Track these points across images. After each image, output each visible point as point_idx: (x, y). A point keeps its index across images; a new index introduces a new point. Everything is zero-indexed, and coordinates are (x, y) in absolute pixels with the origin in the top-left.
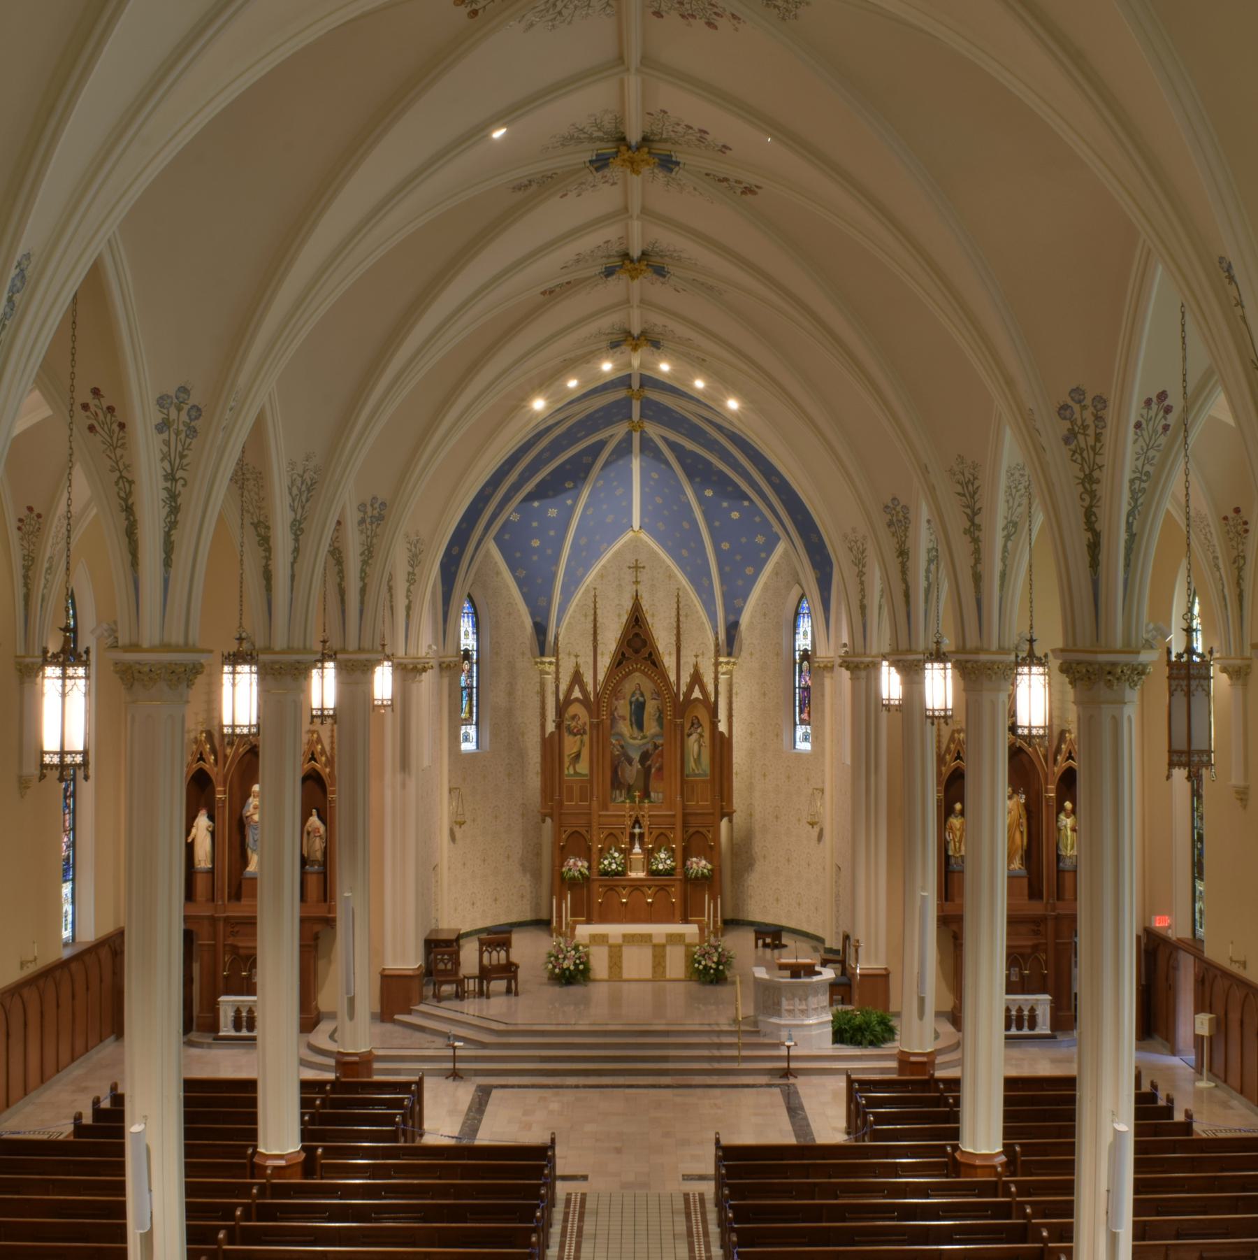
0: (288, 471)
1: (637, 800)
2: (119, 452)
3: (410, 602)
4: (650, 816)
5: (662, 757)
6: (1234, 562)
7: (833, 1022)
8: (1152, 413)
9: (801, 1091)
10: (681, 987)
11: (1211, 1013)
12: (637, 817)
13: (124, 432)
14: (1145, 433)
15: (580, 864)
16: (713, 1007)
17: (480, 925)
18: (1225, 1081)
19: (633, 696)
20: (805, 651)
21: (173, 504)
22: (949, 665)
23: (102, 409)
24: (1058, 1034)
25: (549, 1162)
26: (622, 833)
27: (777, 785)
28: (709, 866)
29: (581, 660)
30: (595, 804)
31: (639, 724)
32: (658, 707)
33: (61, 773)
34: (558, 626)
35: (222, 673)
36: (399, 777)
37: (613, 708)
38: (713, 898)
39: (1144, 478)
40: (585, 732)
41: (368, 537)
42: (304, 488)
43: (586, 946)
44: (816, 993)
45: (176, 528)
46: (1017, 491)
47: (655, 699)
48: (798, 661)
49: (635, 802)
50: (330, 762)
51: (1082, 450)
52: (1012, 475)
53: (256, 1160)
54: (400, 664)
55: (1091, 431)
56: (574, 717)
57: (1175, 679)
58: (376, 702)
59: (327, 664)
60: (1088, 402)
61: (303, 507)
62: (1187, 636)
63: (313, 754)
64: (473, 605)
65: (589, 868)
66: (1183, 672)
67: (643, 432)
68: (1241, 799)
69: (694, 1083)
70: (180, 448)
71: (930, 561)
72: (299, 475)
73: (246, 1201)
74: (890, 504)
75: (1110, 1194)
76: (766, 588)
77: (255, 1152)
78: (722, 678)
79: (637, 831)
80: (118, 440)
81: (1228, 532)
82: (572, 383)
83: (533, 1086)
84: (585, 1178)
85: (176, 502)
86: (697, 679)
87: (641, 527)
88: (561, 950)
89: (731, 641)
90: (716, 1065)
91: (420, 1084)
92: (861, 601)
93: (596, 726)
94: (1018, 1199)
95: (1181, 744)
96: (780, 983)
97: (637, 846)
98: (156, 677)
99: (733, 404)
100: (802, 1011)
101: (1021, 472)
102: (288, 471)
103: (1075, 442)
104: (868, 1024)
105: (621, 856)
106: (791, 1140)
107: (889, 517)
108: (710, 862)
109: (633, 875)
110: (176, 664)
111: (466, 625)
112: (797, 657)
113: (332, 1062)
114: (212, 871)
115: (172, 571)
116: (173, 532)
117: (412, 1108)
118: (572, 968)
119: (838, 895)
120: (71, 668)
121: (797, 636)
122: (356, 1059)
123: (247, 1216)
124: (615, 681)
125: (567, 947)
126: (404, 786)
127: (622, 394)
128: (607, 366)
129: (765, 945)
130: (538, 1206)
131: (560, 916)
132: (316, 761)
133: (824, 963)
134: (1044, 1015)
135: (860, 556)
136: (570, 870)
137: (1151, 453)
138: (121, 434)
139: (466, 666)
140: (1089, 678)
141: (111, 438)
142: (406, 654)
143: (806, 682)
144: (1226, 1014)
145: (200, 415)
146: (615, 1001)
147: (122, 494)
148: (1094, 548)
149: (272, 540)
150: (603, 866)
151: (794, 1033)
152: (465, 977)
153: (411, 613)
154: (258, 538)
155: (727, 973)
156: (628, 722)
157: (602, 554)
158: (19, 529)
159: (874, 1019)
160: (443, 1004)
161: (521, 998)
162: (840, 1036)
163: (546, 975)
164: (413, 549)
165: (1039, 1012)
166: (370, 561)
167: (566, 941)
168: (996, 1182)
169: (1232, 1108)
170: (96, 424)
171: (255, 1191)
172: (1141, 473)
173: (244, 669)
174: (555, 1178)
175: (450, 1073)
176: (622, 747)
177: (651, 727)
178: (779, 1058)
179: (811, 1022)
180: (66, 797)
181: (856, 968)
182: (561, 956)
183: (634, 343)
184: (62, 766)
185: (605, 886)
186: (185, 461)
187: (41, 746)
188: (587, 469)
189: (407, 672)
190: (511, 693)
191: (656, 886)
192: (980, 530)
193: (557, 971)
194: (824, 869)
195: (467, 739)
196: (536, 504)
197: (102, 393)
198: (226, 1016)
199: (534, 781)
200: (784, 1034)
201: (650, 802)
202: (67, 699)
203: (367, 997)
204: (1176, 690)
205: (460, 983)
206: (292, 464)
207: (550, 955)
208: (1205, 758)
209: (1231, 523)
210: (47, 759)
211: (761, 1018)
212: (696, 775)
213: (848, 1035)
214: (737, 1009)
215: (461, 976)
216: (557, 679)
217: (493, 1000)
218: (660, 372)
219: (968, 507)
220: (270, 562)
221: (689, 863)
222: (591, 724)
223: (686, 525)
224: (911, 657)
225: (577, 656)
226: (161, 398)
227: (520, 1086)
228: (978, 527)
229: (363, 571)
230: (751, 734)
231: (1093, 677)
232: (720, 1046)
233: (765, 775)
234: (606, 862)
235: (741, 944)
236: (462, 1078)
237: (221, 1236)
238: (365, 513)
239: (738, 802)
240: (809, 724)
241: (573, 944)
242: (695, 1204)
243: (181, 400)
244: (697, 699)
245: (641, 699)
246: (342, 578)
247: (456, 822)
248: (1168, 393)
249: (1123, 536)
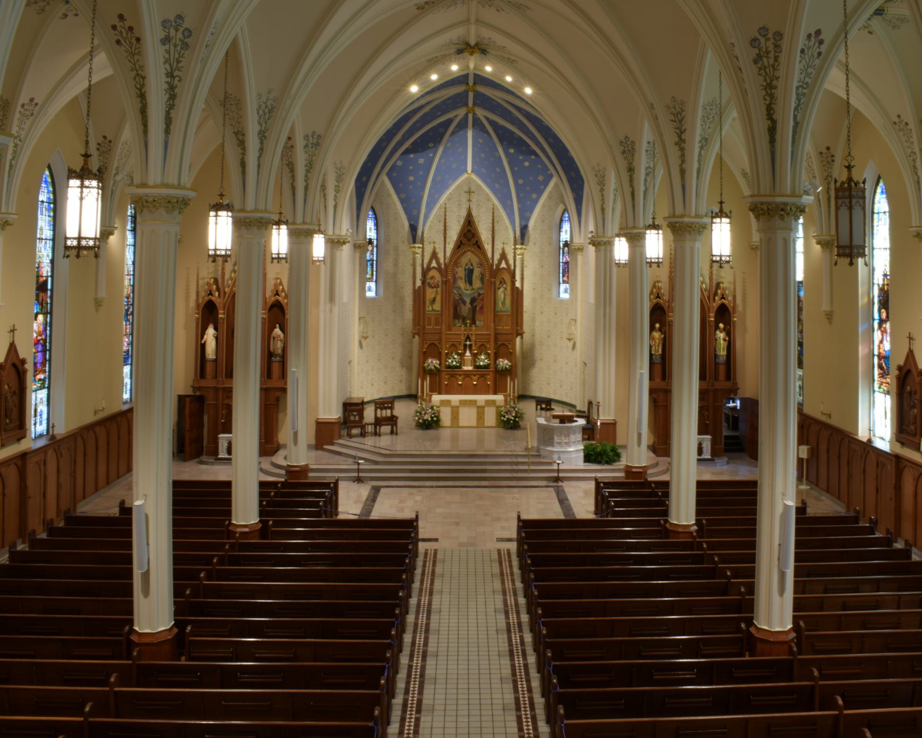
0: (257, 100)
1: (468, 325)
2: (136, 57)
3: (336, 203)
4: (476, 334)
6: (826, 179)
7: (584, 450)
8: (811, 44)
9: (566, 489)
10: (493, 431)
11: (808, 445)
13: (139, 44)
14: (806, 57)
16: (512, 443)
17: (376, 397)
18: (817, 485)
20: (566, 242)
21: (172, 93)
22: (661, 232)
23: (125, 29)
24: (715, 458)
25: (415, 530)
27: (549, 318)
28: (510, 364)
29: (437, 246)
30: (444, 327)
31: (469, 281)
33: (78, 252)
34: (424, 225)
35: (209, 216)
36: (328, 306)
38: (512, 379)
39: (805, 86)
41: (309, 155)
42: (267, 111)
43: (438, 407)
44: (574, 433)
45: (173, 109)
46: (708, 119)
49: (467, 326)
50: (286, 297)
51: (765, 67)
52: (705, 109)
53: (231, 528)
54: (330, 239)
55: (772, 55)
56: (432, 278)
57: (841, 198)
58: (314, 259)
59: (282, 227)
60: (770, 35)
61: (266, 123)
62: (848, 171)
63: (277, 291)
64: (375, 213)
65: (440, 364)
66: (847, 194)
67: (474, 114)
68: (829, 319)
69: (501, 485)
70: (177, 56)
71: (647, 175)
72: (264, 102)
73: (221, 553)
74: (624, 141)
75: (781, 547)
76: (544, 206)
77: (230, 524)
78: (518, 257)
79: (468, 343)
80: (135, 49)
81: (822, 161)
82: (434, 77)
83: (406, 487)
84: (436, 540)
85: (173, 91)
86: (503, 256)
87: (472, 172)
88: (423, 409)
89: (523, 236)
90: (515, 475)
91: (336, 484)
92: (602, 206)
93: (445, 283)
94: (708, 552)
95: (845, 241)
96: (553, 426)
98: (158, 205)
99: (528, 91)
100: (566, 443)
101: (711, 107)
102: (257, 100)
103: (761, 62)
104: (605, 451)
106: (562, 517)
107: (623, 148)
108: (510, 362)
109: (465, 368)
110: (171, 197)
111: (370, 224)
113: (283, 472)
114: (215, 361)
115: (171, 137)
116: (171, 111)
117: (331, 498)
118: (430, 419)
119: (584, 380)
120: (87, 181)
121: (561, 233)
122: (298, 469)
123: (221, 561)
126: (331, 310)
127: (460, 89)
128: (455, 68)
129: (542, 409)
130: (407, 556)
131: (423, 392)
132: (279, 296)
133: (578, 416)
134: (707, 447)
136: (429, 365)
137: (810, 70)
138: (138, 45)
139: (370, 248)
140: (769, 214)
141: (131, 48)
142: (333, 233)
144: (818, 445)
145: (191, 35)
146: (455, 438)
147: (138, 86)
148: (772, 130)
149: (246, 142)
151: (562, 456)
152: (366, 424)
153: (337, 209)
154: (237, 142)
155: (521, 423)
156: (463, 281)
157: (449, 186)
158: (98, 149)
159: (608, 448)
160: (352, 440)
161: (399, 437)
162: (588, 458)
163: (414, 424)
165: (704, 445)
166: (311, 170)
167: (426, 404)
168: (692, 542)
169: (822, 501)
170: (121, 39)
171: (227, 547)
172: (803, 83)
173: (223, 213)
174: (418, 540)
175: (355, 479)
176: (460, 295)
177: (477, 284)
178: (552, 471)
179: (571, 449)
180: (127, 315)
181: (597, 420)
182: (423, 412)
183: (471, 50)
184: (79, 248)
185: (450, 374)
186: (180, 65)
187: (65, 234)
188: (442, 136)
189: (334, 243)
190: (396, 264)
191: (479, 375)
192: (685, 143)
193: (421, 421)
194: (576, 365)
195: (370, 290)
196: (412, 156)
197: (125, 17)
198: (223, 446)
199: (409, 315)
200: (555, 456)
201: (476, 326)
202: (84, 201)
203: (307, 434)
204: (841, 206)
205: (363, 427)
206: (260, 95)
207: (417, 412)
208: (861, 251)
209: (824, 156)
210: (69, 243)
211: (542, 447)
212: (502, 311)
213: (593, 458)
214: (527, 442)
215: (364, 423)
216: (423, 256)
217: (382, 438)
218: (485, 72)
219: (678, 128)
220: (244, 157)
221: (498, 362)
222: (442, 281)
224: (635, 231)
225: (434, 243)
226: (165, 21)
227: (397, 487)
228: (684, 141)
229: (306, 176)
230: (534, 289)
231: (771, 213)
232: (517, 464)
233: (542, 313)
234: (450, 361)
235: (529, 408)
236: (363, 482)
237: (202, 575)
238: (308, 141)
239: (526, 327)
240: (568, 283)
241: (430, 406)
242: (504, 556)
243: (178, 23)
244: (503, 268)
245: (471, 267)
246: (294, 180)
247: (363, 337)
248: (822, 31)
249: (792, 123)
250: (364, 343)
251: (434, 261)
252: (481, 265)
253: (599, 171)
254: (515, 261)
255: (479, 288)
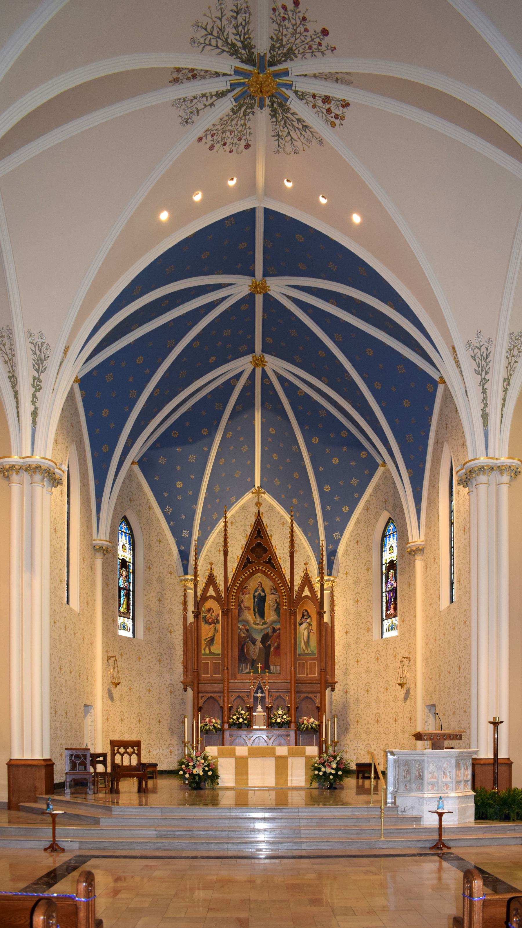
5: (280, 639)
12: (259, 684)
15: (214, 721)
19: (256, 591)
26: (248, 696)
28: (317, 723)
31: (260, 612)
32: (276, 600)
36: (26, 576)
37: (240, 601)
40: (218, 622)
47: (273, 594)
48: (384, 572)
56: (209, 610)
86: (307, 580)
93: (225, 613)
97: (259, 706)
105: (247, 714)
112: (384, 569)
118: (201, 773)
124: (239, 582)
125: (197, 757)
135: (483, 362)
143: (392, 585)
150: (232, 720)
156: (252, 611)
164: (38, 353)
176: (247, 631)
177: (271, 616)
182: (191, 764)
196: (179, 449)
216: (196, 586)
223: (296, 475)
234: (235, 717)
244: (306, 596)
245: (263, 594)
250: (116, 692)
251: (211, 589)
252: (276, 590)
253: (479, 349)
254: (322, 590)
255: (274, 622)
